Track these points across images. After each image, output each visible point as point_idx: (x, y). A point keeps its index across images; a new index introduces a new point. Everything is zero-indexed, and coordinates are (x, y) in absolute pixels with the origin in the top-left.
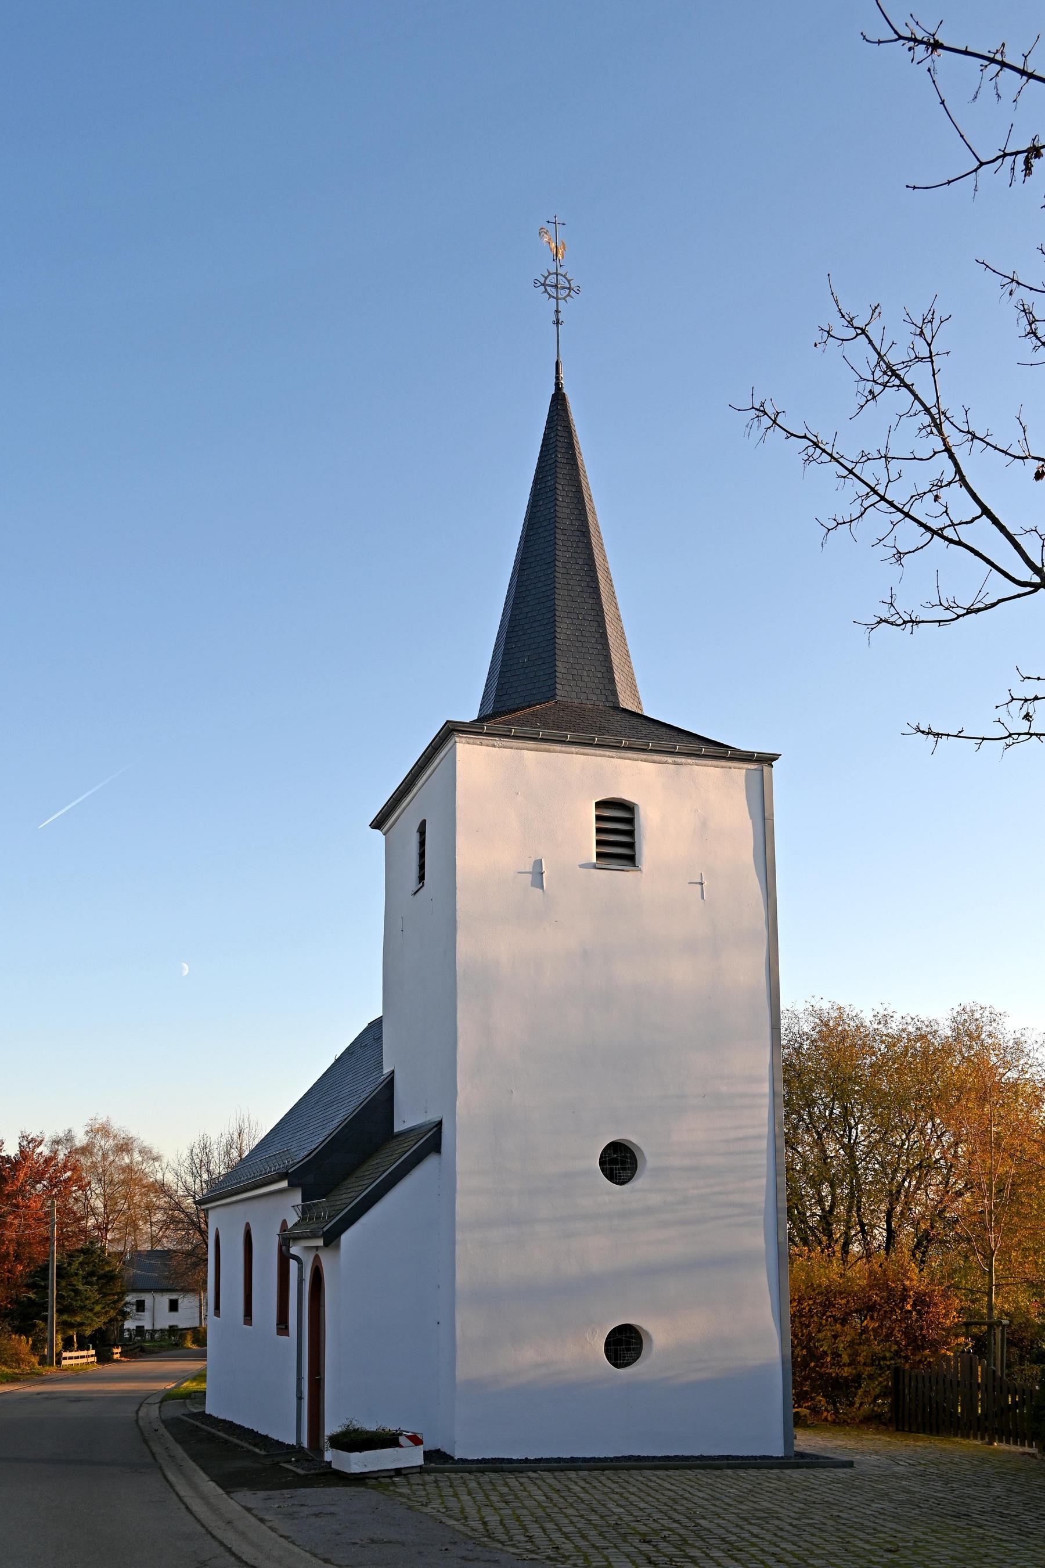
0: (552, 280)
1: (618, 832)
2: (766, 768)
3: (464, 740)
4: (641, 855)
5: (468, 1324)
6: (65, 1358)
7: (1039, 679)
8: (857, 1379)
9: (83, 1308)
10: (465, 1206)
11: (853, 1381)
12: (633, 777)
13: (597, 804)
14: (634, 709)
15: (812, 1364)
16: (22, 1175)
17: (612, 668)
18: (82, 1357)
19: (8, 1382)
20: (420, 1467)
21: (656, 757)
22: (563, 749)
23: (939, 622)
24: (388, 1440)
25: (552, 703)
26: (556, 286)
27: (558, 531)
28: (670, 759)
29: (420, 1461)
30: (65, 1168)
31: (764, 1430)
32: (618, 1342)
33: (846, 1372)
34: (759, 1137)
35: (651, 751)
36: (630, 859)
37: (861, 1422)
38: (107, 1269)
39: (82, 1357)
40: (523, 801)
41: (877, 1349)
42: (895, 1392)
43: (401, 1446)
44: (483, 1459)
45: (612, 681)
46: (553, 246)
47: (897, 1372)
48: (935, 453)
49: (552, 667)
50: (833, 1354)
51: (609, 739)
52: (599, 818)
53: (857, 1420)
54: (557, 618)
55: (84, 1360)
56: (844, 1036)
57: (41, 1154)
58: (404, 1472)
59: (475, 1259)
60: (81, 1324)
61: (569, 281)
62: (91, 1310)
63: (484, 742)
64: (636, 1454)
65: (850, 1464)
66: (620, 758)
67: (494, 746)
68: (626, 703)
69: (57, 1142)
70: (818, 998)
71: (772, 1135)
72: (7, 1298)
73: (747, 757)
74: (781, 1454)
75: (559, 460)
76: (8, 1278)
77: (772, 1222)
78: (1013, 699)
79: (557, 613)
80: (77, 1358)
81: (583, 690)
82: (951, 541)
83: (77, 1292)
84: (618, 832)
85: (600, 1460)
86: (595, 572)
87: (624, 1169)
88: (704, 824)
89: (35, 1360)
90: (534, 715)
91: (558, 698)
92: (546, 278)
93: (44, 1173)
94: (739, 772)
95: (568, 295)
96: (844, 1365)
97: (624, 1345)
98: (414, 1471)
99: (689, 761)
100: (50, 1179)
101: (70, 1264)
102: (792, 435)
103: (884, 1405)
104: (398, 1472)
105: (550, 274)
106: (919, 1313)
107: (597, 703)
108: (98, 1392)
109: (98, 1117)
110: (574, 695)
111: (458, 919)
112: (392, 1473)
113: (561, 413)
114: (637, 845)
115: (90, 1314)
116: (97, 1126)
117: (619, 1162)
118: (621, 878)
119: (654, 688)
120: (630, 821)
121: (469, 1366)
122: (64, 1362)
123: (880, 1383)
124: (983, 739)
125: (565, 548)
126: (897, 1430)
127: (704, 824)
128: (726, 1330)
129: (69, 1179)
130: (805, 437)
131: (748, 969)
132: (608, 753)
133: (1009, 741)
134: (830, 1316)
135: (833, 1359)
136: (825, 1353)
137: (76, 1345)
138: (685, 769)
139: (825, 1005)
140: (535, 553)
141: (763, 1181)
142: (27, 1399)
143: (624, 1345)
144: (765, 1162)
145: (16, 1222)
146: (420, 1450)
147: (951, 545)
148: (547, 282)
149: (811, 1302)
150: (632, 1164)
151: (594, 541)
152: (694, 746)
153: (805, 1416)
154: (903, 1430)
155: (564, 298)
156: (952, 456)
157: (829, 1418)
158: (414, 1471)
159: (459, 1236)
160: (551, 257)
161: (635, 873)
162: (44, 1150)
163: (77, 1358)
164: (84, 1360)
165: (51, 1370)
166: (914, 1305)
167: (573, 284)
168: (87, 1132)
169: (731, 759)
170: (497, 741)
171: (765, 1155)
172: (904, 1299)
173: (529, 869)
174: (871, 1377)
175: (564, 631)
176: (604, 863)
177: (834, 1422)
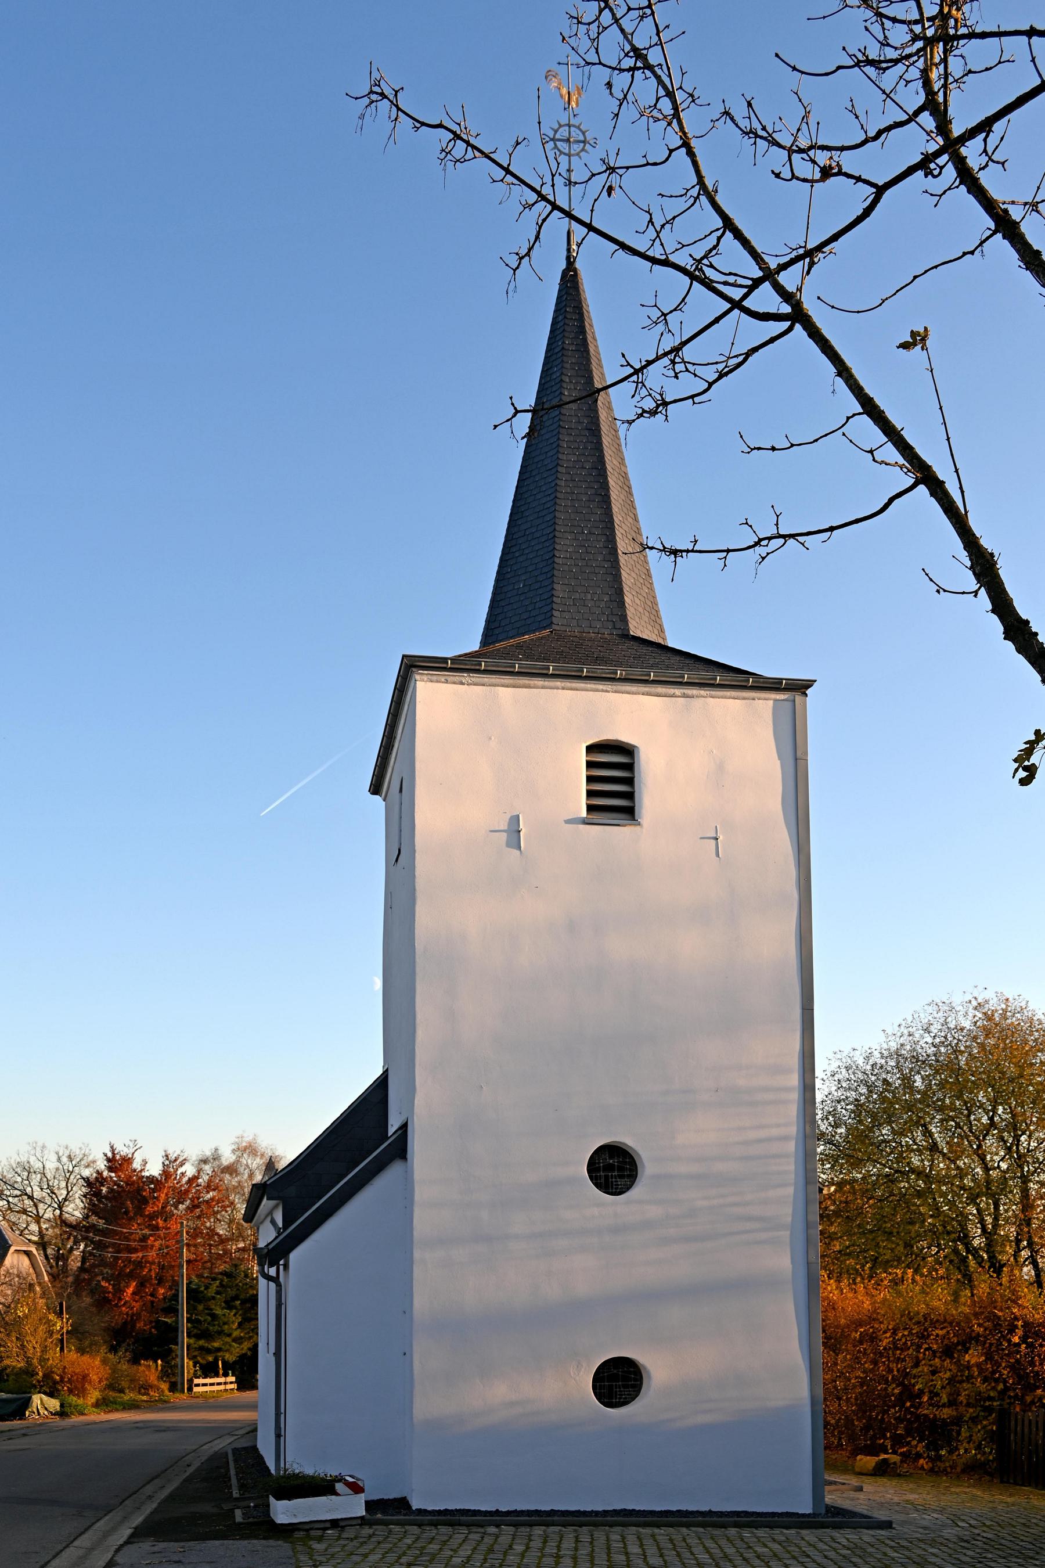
0: (563, 133)
1: (614, 781)
2: (799, 698)
3: (425, 678)
4: (641, 807)
5: (427, 1357)
6: (198, 1385)
7: (773, 449)
8: (958, 1421)
9: (220, 1333)
10: (423, 1221)
11: (952, 1423)
12: (631, 713)
13: (587, 747)
14: (653, 638)
15: (908, 1404)
16: (163, 1196)
17: (621, 590)
18: (219, 1384)
19: (124, 1409)
20: (362, 1518)
21: (661, 689)
22: (546, 683)
23: (692, 397)
24: (323, 1487)
25: (546, 632)
26: (568, 140)
27: (562, 431)
28: (678, 691)
29: (362, 1512)
30: (208, 1187)
31: (789, 1484)
32: (613, 1378)
33: (946, 1413)
34: (785, 1138)
35: (654, 682)
36: (629, 813)
37: (963, 1471)
38: (251, 1292)
39: (219, 1384)
40: (508, 746)
41: (983, 1387)
42: (999, 1438)
43: (337, 1494)
44: (446, 1510)
45: (622, 604)
46: (564, 91)
47: (1004, 1416)
48: (671, 151)
49: (560, 596)
50: (931, 1392)
51: (601, 669)
52: (590, 765)
53: (959, 1470)
54: (557, 534)
55: (222, 1387)
56: (1015, 1029)
57: (183, 1174)
58: (342, 1524)
59: (439, 1282)
60: (219, 1350)
61: (584, 133)
62: (229, 1335)
63: (450, 679)
64: (630, 1507)
65: (888, 1525)
66: (616, 692)
67: (462, 683)
68: (638, 627)
69: (205, 1161)
70: (981, 988)
71: (801, 1135)
72: (151, 1322)
73: (773, 685)
74: (808, 1510)
75: (566, 347)
76: (152, 1302)
77: (801, 1237)
78: (517, 412)
79: (557, 528)
80: (212, 1384)
81: (586, 616)
82: (654, 261)
83: (214, 1317)
84: (614, 781)
85: (584, 1513)
86: (606, 477)
87: (621, 1177)
88: (721, 768)
89: (164, 1386)
90: (519, 646)
91: (554, 627)
92: (556, 131)
93: (187, 1191)
94: (765, 704)
95: (583, 150)
96: (944, 1405)
97: (618, 1381)
98: (354, 1522)
99: (702, 692)
100: (192, 1200)
101: (207, 1288)
102: (423, 124)
103: (990, 1452)
104: (335, 1523)
105: (560, 126)
106: (1030, 1346)
107: (602, 631)
108: (189, 1421)
109: (245, 1135)
110: (574, 623)
111: (417, 887)
112: (328, 1525)
113: (571, 291)
114: (636, 794)
115: (228, 1339)
116: (244, 1144)
117: (613, 1169)
118: (616, 835)
119: (681, 610)
120: (630, 767)
121: (429, 1404)
122: (196, 1389)
123: (984, 1427)
124: (728, 551)
125: (570, 451)
126: (1002, 1482)
127: (721, 768)
128: (743, 1362)
129: (212, 1199)
130: (440, 126)
131: (776, 939)
132: (601, 687)
133: (761, 550)
134: (926, 1349)
135: (931, 1398)
136: (921, 1392)
137: (221, 1372)
138: (698, 703)
139: (989, 995)
140: (536, 460)
141: (791, 1190)
142: (116, 1428)
143: (618, 1381)
144: (792, 1167)
145: (157, 1244)
146: (362, 1498)
147: (656, 267)
148: (558, 136)
149: (906, 1333)
150: (630, 1170)
151: (606, 441)
152: (705, 674)
153: (895, 1463)
154: (1008, 1482)
155: (578, 154)
156: (691, 153)
157: (926, 1467)
158: (354, 1522)
159: (417, 1254)
160: (562, 104)
161: (632, 828)
162: (189, 1170)
163: (212, 1384)
164: (222, 1387)
165: (182, 1397)
166: (1024, 1339)
167: (589, 136)
168: (234, 1151)
169: (753, 688)
170: (465, 677)
171: (792, 1160)
172: (1012, 1329)
173: (504, 826)
174: (974, 1420)
175: (565, 548)
176: (596, 817)
177: (932, 1471)
